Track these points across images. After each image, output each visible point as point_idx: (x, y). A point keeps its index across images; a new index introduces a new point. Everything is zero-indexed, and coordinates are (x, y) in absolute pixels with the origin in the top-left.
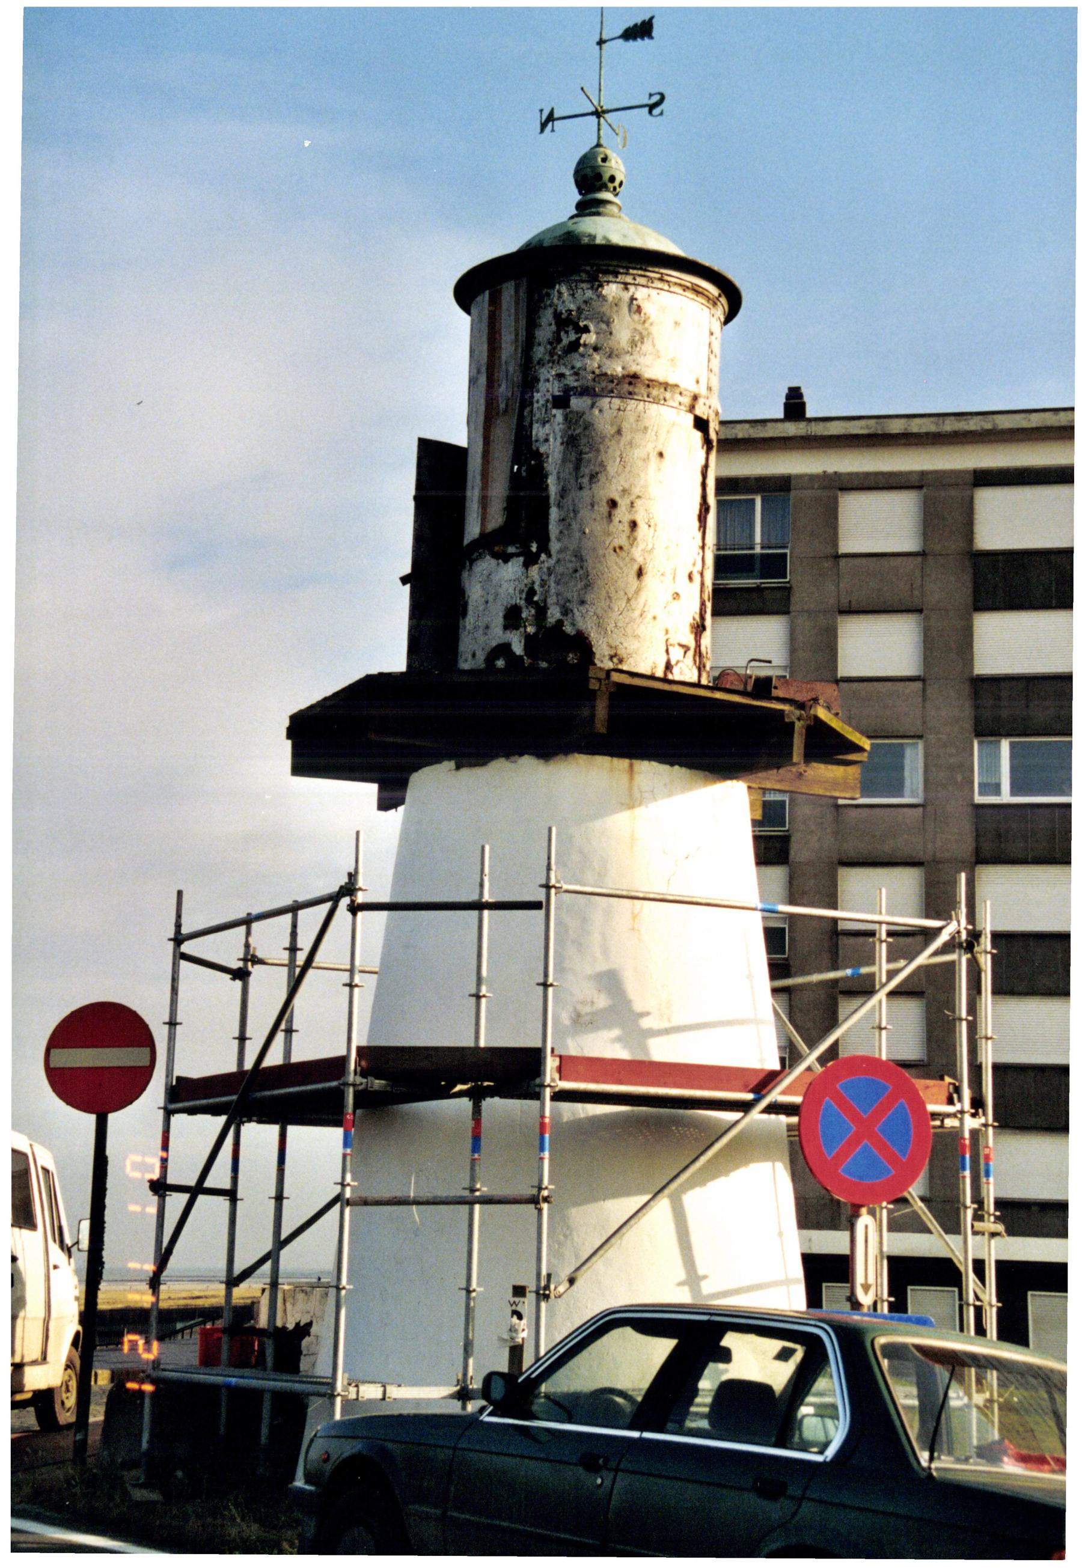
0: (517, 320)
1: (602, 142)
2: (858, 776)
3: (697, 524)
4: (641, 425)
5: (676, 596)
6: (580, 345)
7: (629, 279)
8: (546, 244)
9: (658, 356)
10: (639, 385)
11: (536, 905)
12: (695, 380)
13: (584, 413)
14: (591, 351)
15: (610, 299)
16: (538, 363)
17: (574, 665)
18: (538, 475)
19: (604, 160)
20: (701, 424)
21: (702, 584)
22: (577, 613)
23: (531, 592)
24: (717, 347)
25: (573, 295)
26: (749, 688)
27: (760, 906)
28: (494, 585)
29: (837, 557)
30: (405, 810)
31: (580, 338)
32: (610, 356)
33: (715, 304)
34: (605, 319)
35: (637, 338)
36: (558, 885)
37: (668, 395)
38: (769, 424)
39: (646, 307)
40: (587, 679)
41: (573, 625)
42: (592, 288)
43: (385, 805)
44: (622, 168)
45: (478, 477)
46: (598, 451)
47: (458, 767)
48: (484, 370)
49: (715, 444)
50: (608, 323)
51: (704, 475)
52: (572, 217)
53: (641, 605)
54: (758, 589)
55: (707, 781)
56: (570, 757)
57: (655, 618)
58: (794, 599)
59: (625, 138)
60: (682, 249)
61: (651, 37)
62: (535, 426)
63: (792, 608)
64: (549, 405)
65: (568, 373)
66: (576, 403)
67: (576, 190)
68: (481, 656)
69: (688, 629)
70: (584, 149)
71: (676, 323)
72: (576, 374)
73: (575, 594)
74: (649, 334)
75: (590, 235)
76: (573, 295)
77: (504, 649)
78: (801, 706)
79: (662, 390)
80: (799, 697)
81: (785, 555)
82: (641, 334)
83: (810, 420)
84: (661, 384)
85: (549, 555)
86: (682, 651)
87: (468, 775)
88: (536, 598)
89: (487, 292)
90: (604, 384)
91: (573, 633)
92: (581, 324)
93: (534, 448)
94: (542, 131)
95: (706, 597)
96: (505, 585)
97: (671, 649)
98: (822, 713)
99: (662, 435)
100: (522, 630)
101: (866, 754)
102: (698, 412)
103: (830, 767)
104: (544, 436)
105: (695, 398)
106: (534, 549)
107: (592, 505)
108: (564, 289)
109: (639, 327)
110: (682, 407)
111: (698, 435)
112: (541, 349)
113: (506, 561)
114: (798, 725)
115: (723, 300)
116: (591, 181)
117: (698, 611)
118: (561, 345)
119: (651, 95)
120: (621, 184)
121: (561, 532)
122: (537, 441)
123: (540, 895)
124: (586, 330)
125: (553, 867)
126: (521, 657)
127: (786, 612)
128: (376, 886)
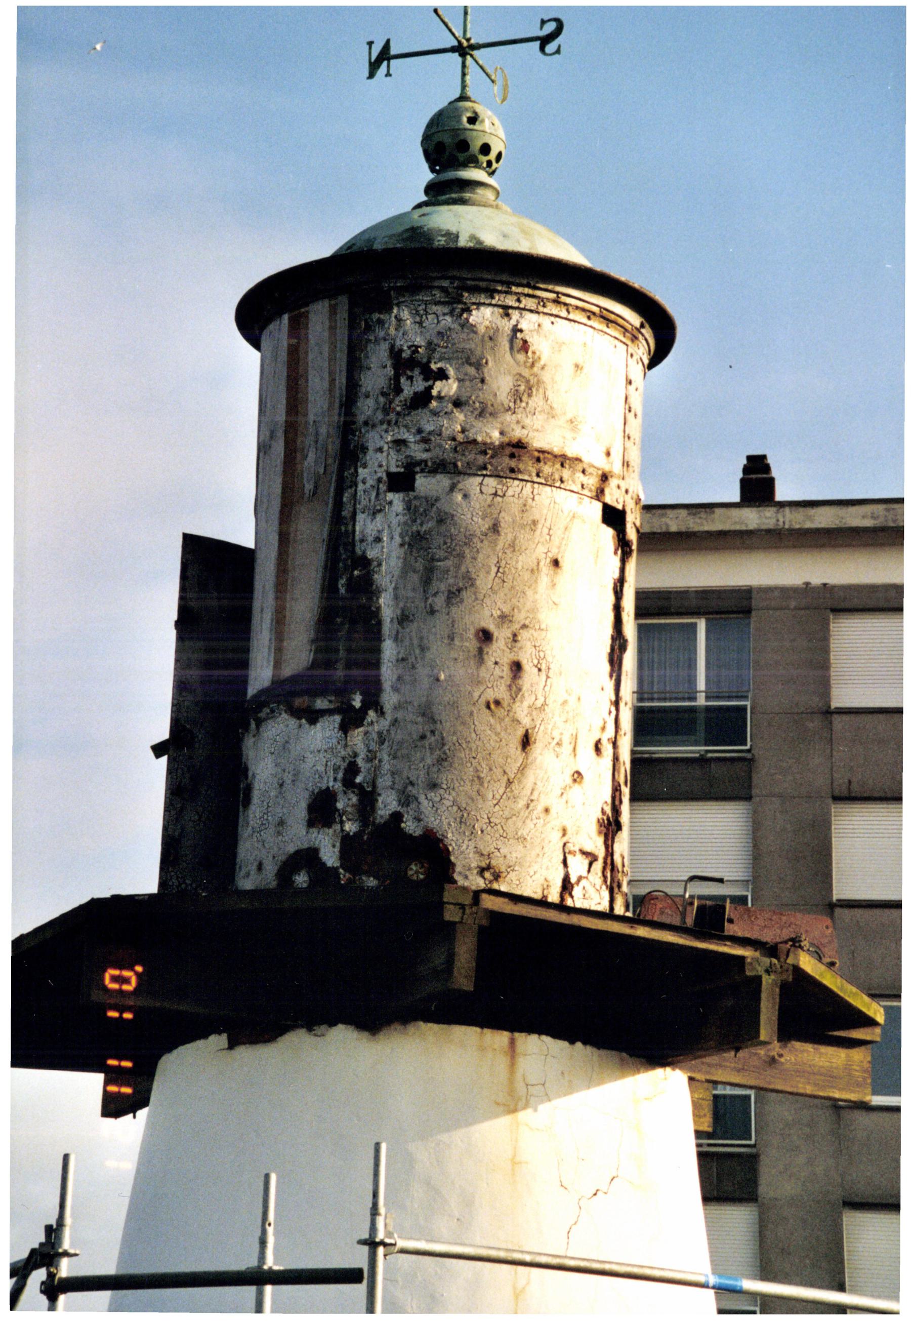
0: (332, 359)
1: (469, 92)
2: (866, 1065)
3: (607, 667)
4: (528, 518)
5: (578, 776)
6: (432, 397)
7: (510, 301)
8: (378, 246)
9: (551, 414)
10: (525, 458)
11: (351, 1276)
12: (605, 450)
13: (437, 499)
14: (450, 406)
15: (481, 329)
16: (366, 423)
17: (419, 883)
18: (365, 587)
19: (473, 120)
20: (613, 517)
21: (616, 759)
22: (425, 803)
23: (352, 769)
24: (637, 402)
25: (420, 323)
26: (690, 921)
27: (712, 1280)
28: (291, 757)
29: (828, 713)
30: (150, 1112)
31: (431, 387)
32: (481, 414)
33: (634, 338)
34: (473, 360)
35: (522, 388)
36: (388, 1241)
37: (566, 473)
38: (718, 511)
39: (538, 344)
40: (440, 905)
41: (418, 820)
42: (451, 313)
43: (114, 1107)
44: (501, 133)
45: (271, 596)
46: (461, 556)
47: (232, 1045)
48: (280, 434)
49: (634, 547)
50: (478, 366)
51: (618, 593)
52: (419, 206)
53: (527, 792)
54: (702, 761)
55: (625, 1069)
56: (411, 1028)
57: (547, 810)
58: (758, 778)
59: (505, 87)
60: (587, 257)
62: (360, 517)
63: (755, 791)
64: (383, 487)
65: (411, 439)
66: (422, 483)
67: (425, 166)
68: (270, 869)
69: (593, 828)
70: (441, 103)
71: (577, 366)
72: (425, 441)
73: (422, 773)
74: (539, 382)
75: (448, 234)
76: (420, 323)
77: (307, 858)
78: (771, 950)
79: (558, 466)
80: (768, 936)
81: (743, 709)
82: (528, 381)
83: (782, 505)
84: (556, 456)
85: (381, 713)
86: (586, 862)
87: (245, 1053)
88: (358, 780)
89: (286, 317)
90: (470, 457)
91: (418, 833)
92: (433, 366)
93: (359, 552)
94: (371, 75)
95: (622, 780)
96: (311, 759)
97: (569, 857)
98: (807, 963)
99: (557, 533)
100: (337, 827)
101: (878, 1030)
102: (608, 499)
103: (824, 1049)
104: (374, 533)
105: (605, 478)
106: (357, 703)
107: (451, 638)
108: (405, 314)
109: (526, 373)
110: (586, 492)
111: (609, 533)
112: (370, 402)
113: (313, 721)
114: (767, 981)
115: (647, 332)
116: (450, 151)
117: (609, 801)
118: (402, 397)
119: (543, 22)
120: (499, 157)
121: (399, 678)
122: (362, 541)
123: (358, 1259)
124: (442, 375)
125: (382, 1210)
126: (335, 869)
127: (748, 798)
128: (93, 1247)
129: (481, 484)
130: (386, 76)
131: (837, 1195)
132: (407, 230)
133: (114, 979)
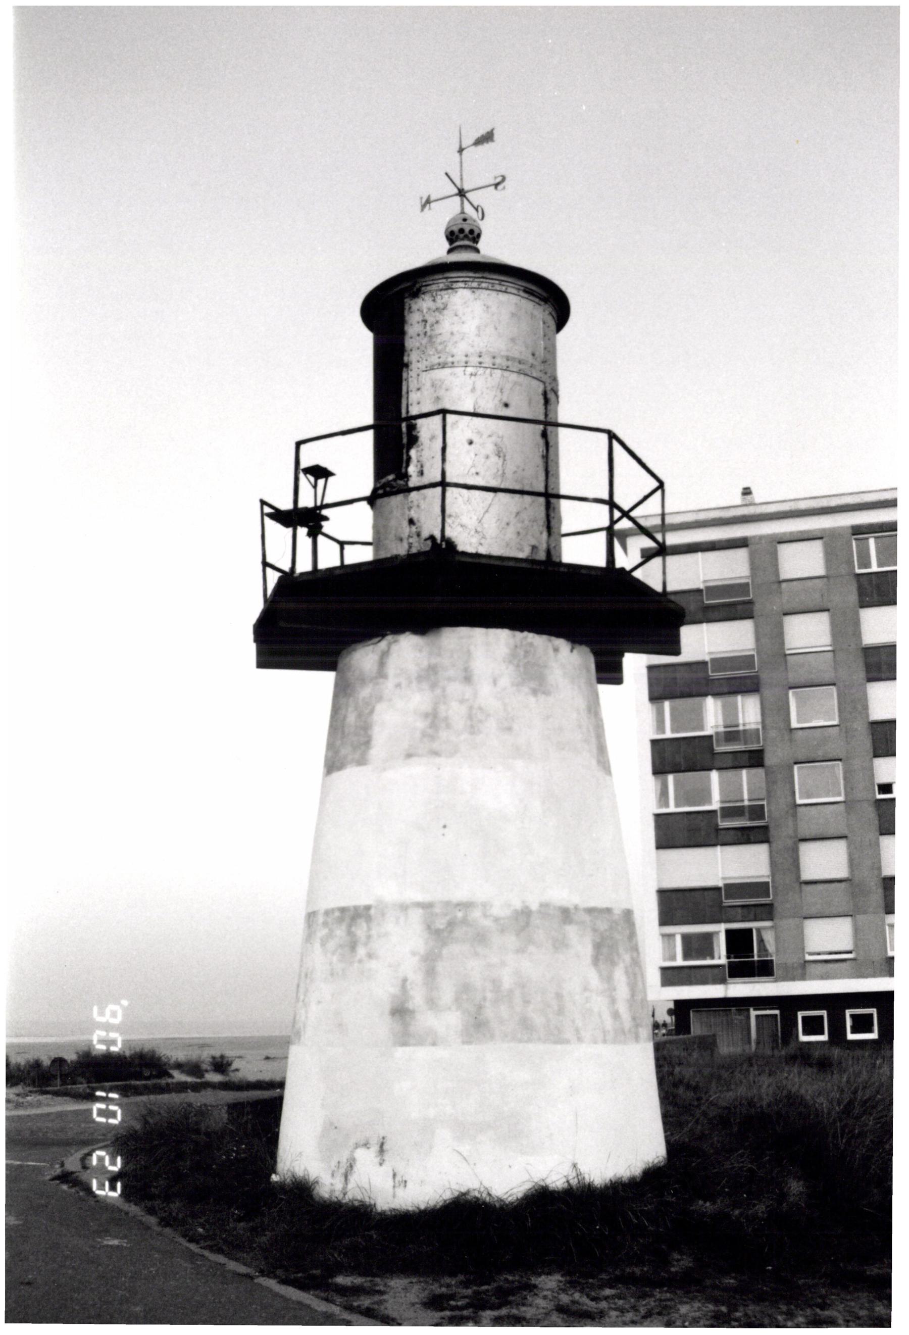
81: (763, 806)
131: (792, 761)
133: (113, 1115)
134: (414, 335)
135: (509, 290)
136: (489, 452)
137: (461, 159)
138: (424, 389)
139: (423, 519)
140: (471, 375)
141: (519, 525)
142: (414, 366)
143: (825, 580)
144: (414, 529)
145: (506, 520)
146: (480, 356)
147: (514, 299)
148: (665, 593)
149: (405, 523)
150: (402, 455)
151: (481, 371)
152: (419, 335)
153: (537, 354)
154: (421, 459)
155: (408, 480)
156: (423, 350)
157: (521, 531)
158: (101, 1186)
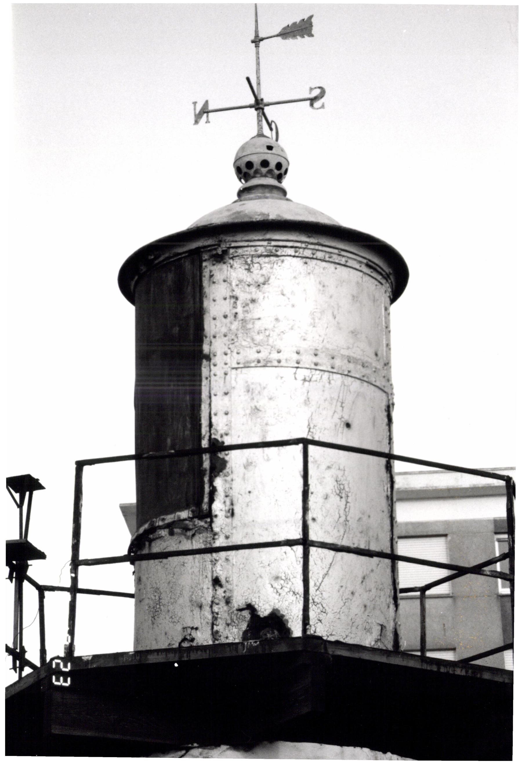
52: (235, 202)
61: (311, 35)
94: (196, 122)
129: (295, 373)
130: (206, 122)
132: (235, 213)
134: (220, 315)
135: (351, 263)
136: (329, 492)
137: (258, 53)
138: (234, 394)
139: (234, 579)
140: (305, 380)
141: (366, 596)
142: (218, 359)
143: (449, 600)
144: (220, 592)
145: (350, 588)
146: (316, 355)
147: (355, 276)
148: (311, 641)
149: (208, 584)
150: (202, 483)
151: (317, 375)
152: (225, 317)
153: (379, 353)
154: (231, 493)
155: (212, 522)
156: (232, 339)
157: (368, 604)
158: (58, 680)
